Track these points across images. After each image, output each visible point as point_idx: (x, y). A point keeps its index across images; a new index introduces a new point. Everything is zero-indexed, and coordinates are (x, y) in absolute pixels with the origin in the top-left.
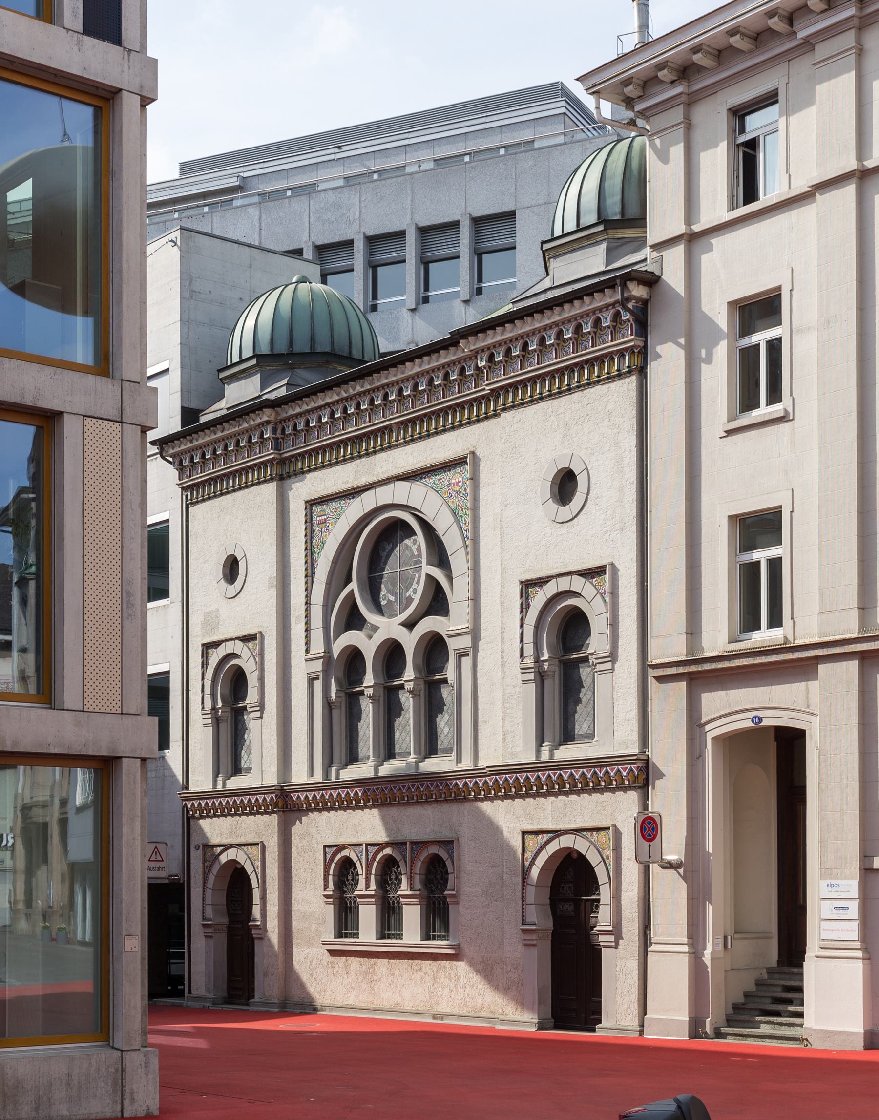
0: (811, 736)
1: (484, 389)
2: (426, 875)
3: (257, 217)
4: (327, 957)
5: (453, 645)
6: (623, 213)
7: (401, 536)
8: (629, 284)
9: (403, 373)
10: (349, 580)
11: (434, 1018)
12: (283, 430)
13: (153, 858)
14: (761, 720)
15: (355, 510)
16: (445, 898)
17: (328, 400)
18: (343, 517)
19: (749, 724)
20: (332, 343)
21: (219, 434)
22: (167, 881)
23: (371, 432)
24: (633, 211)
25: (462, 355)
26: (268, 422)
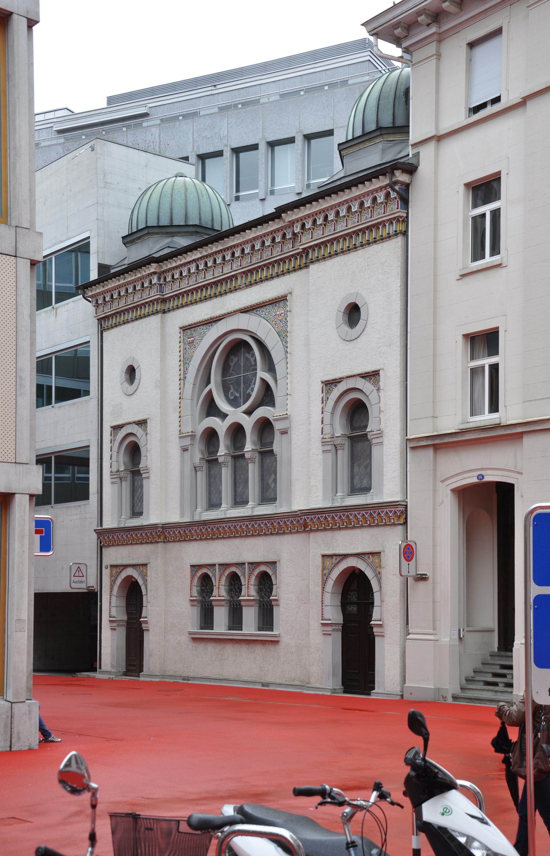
0: (518, 488)
1: (299, 249)
2: (258, 586)
3: (157, 135)
4: (192, 644)
5: (277, 426)
6: (394, 122)
7: (244, 351)
8: (395, 171)
9: (243, 238)
10: (208, 382)
11: (263, 686)
12: (165, 279)
14: (483, 477)
15: (214, 333)
16: (271, 601)
17: (194, 257)
19: (475, 480)
20: (200, 219)
21: (122, 282)
22: (86, 591)
23: (223, 279)
24: (400, 122)
25: (284, 225)
26: (155, 273)
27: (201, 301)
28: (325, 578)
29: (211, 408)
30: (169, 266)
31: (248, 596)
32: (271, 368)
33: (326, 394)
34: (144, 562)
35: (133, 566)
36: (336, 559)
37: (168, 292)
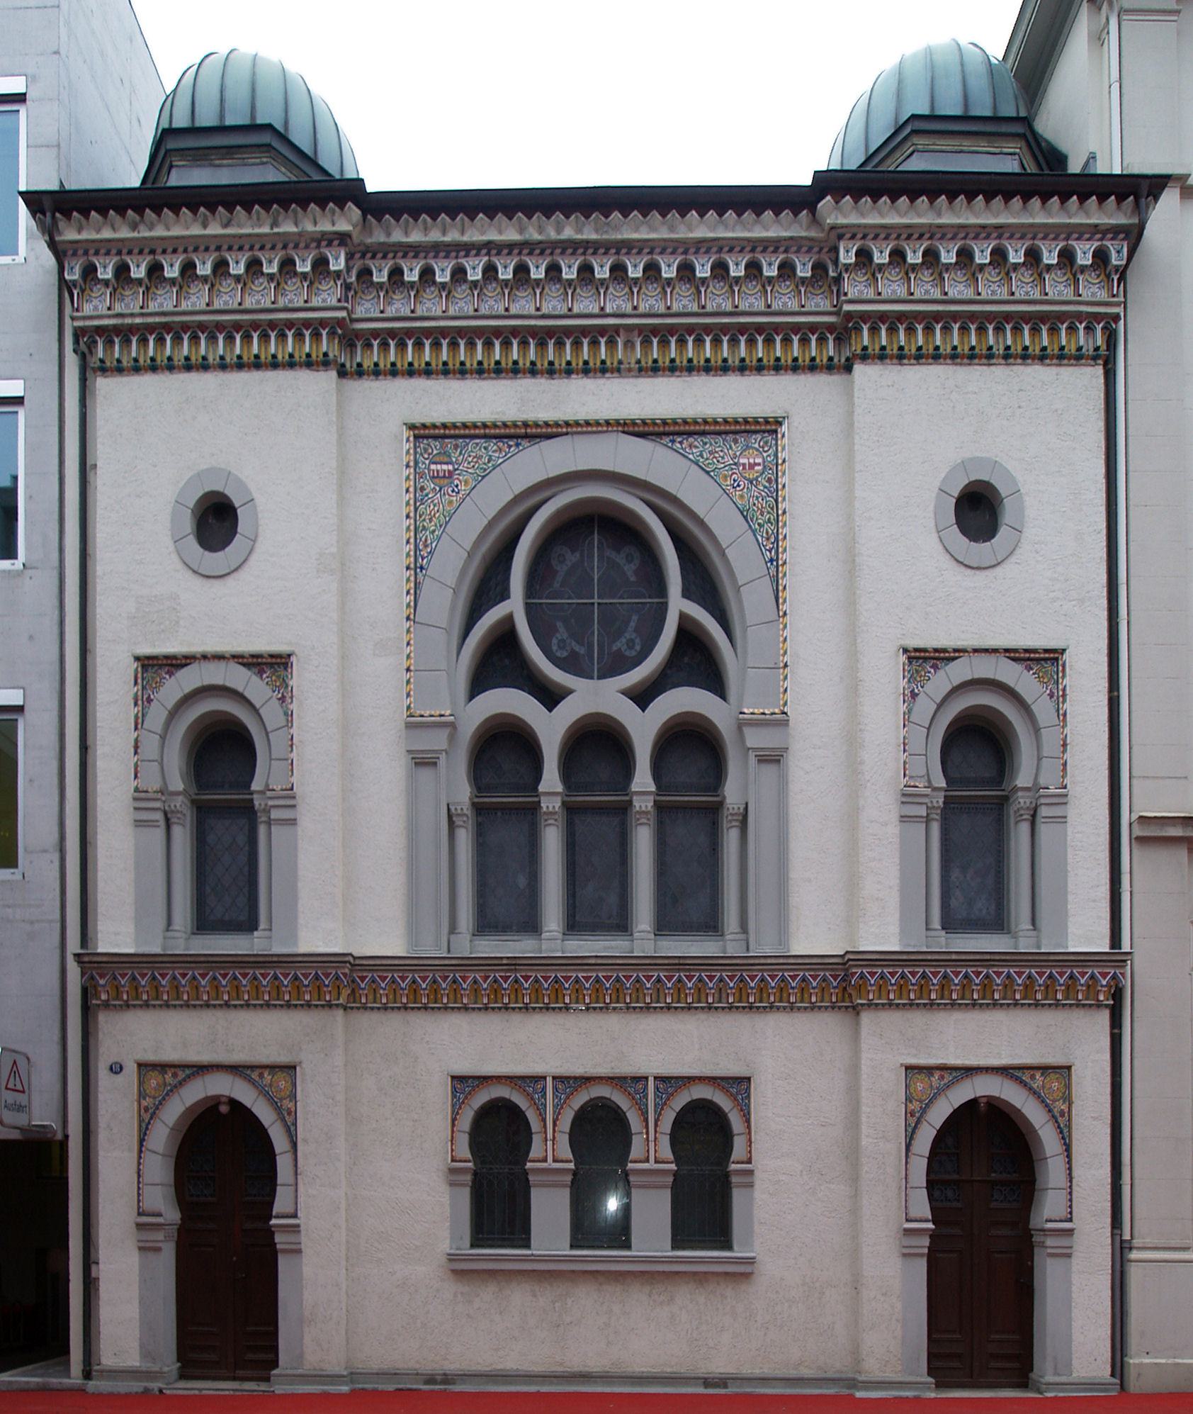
4: (450, 1288)
7: (599, 541)
17: (493, 236)
21: (215, 229)
26: (343, 238)
27: (481, 371)
28: (146, 1117)
29: (499, 662)
30: (398, 236)
31: (555, 1161)
33: (144, 688)
34: (283, 1059)
35: (235, 1069)
36: (942, 1077)
37: (367, 309)
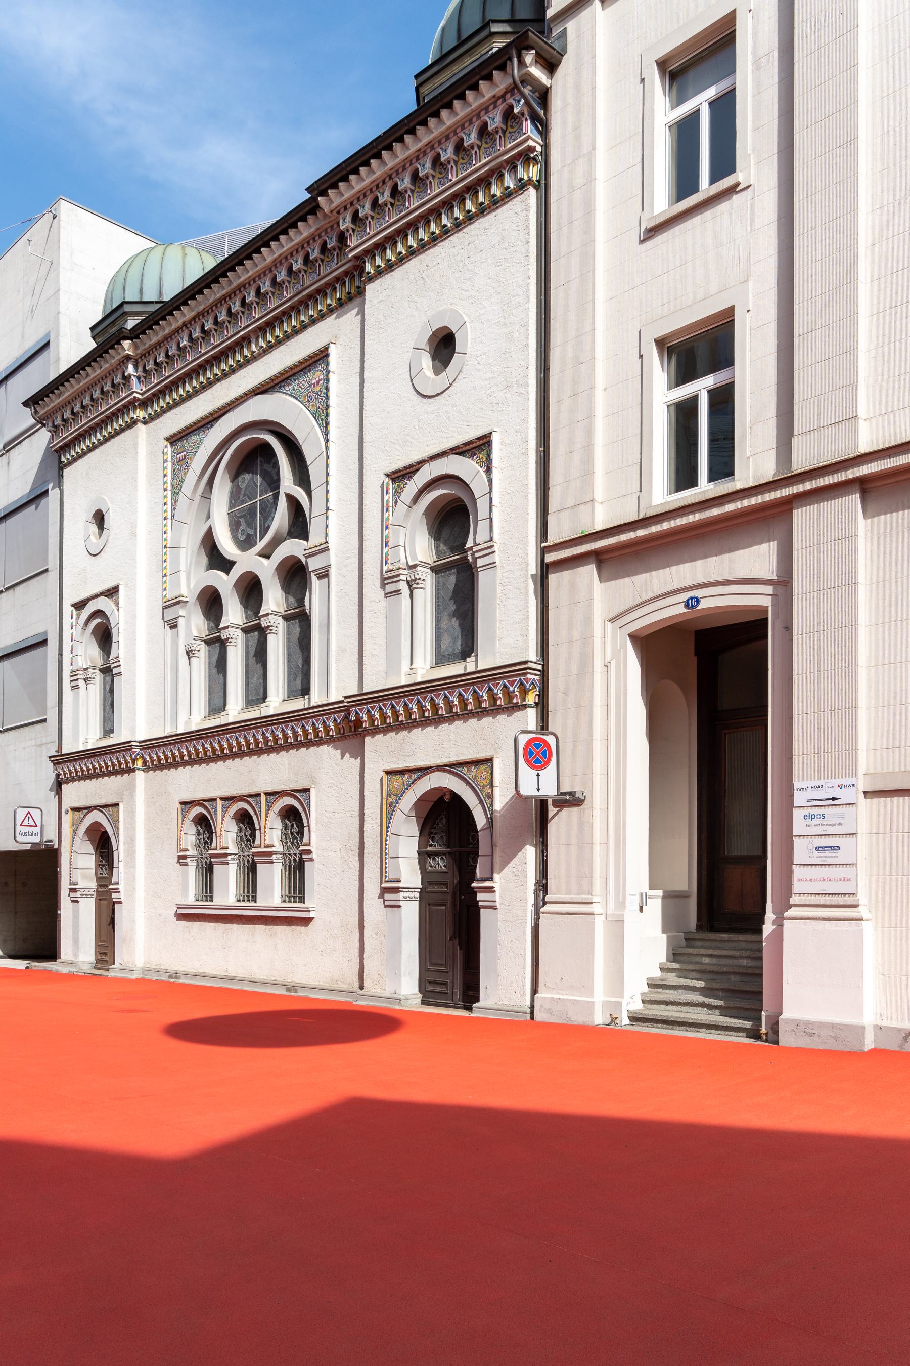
5: (314, 564)
7: (261, 462)
13: (25, 823)
14: (698, 601)
18: (202, 447)
19: (681, 609)
32: (303, 477)
33: (394, 495)
34: (114, 801)
36: (411, 777)
